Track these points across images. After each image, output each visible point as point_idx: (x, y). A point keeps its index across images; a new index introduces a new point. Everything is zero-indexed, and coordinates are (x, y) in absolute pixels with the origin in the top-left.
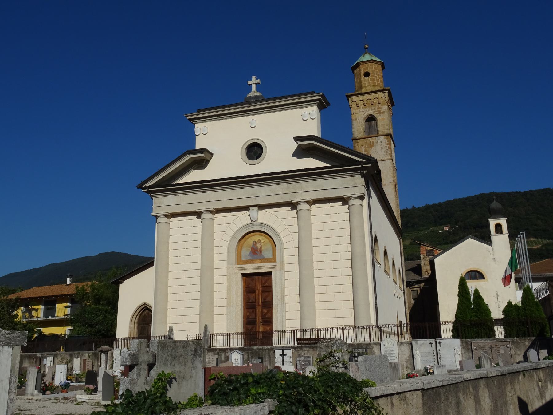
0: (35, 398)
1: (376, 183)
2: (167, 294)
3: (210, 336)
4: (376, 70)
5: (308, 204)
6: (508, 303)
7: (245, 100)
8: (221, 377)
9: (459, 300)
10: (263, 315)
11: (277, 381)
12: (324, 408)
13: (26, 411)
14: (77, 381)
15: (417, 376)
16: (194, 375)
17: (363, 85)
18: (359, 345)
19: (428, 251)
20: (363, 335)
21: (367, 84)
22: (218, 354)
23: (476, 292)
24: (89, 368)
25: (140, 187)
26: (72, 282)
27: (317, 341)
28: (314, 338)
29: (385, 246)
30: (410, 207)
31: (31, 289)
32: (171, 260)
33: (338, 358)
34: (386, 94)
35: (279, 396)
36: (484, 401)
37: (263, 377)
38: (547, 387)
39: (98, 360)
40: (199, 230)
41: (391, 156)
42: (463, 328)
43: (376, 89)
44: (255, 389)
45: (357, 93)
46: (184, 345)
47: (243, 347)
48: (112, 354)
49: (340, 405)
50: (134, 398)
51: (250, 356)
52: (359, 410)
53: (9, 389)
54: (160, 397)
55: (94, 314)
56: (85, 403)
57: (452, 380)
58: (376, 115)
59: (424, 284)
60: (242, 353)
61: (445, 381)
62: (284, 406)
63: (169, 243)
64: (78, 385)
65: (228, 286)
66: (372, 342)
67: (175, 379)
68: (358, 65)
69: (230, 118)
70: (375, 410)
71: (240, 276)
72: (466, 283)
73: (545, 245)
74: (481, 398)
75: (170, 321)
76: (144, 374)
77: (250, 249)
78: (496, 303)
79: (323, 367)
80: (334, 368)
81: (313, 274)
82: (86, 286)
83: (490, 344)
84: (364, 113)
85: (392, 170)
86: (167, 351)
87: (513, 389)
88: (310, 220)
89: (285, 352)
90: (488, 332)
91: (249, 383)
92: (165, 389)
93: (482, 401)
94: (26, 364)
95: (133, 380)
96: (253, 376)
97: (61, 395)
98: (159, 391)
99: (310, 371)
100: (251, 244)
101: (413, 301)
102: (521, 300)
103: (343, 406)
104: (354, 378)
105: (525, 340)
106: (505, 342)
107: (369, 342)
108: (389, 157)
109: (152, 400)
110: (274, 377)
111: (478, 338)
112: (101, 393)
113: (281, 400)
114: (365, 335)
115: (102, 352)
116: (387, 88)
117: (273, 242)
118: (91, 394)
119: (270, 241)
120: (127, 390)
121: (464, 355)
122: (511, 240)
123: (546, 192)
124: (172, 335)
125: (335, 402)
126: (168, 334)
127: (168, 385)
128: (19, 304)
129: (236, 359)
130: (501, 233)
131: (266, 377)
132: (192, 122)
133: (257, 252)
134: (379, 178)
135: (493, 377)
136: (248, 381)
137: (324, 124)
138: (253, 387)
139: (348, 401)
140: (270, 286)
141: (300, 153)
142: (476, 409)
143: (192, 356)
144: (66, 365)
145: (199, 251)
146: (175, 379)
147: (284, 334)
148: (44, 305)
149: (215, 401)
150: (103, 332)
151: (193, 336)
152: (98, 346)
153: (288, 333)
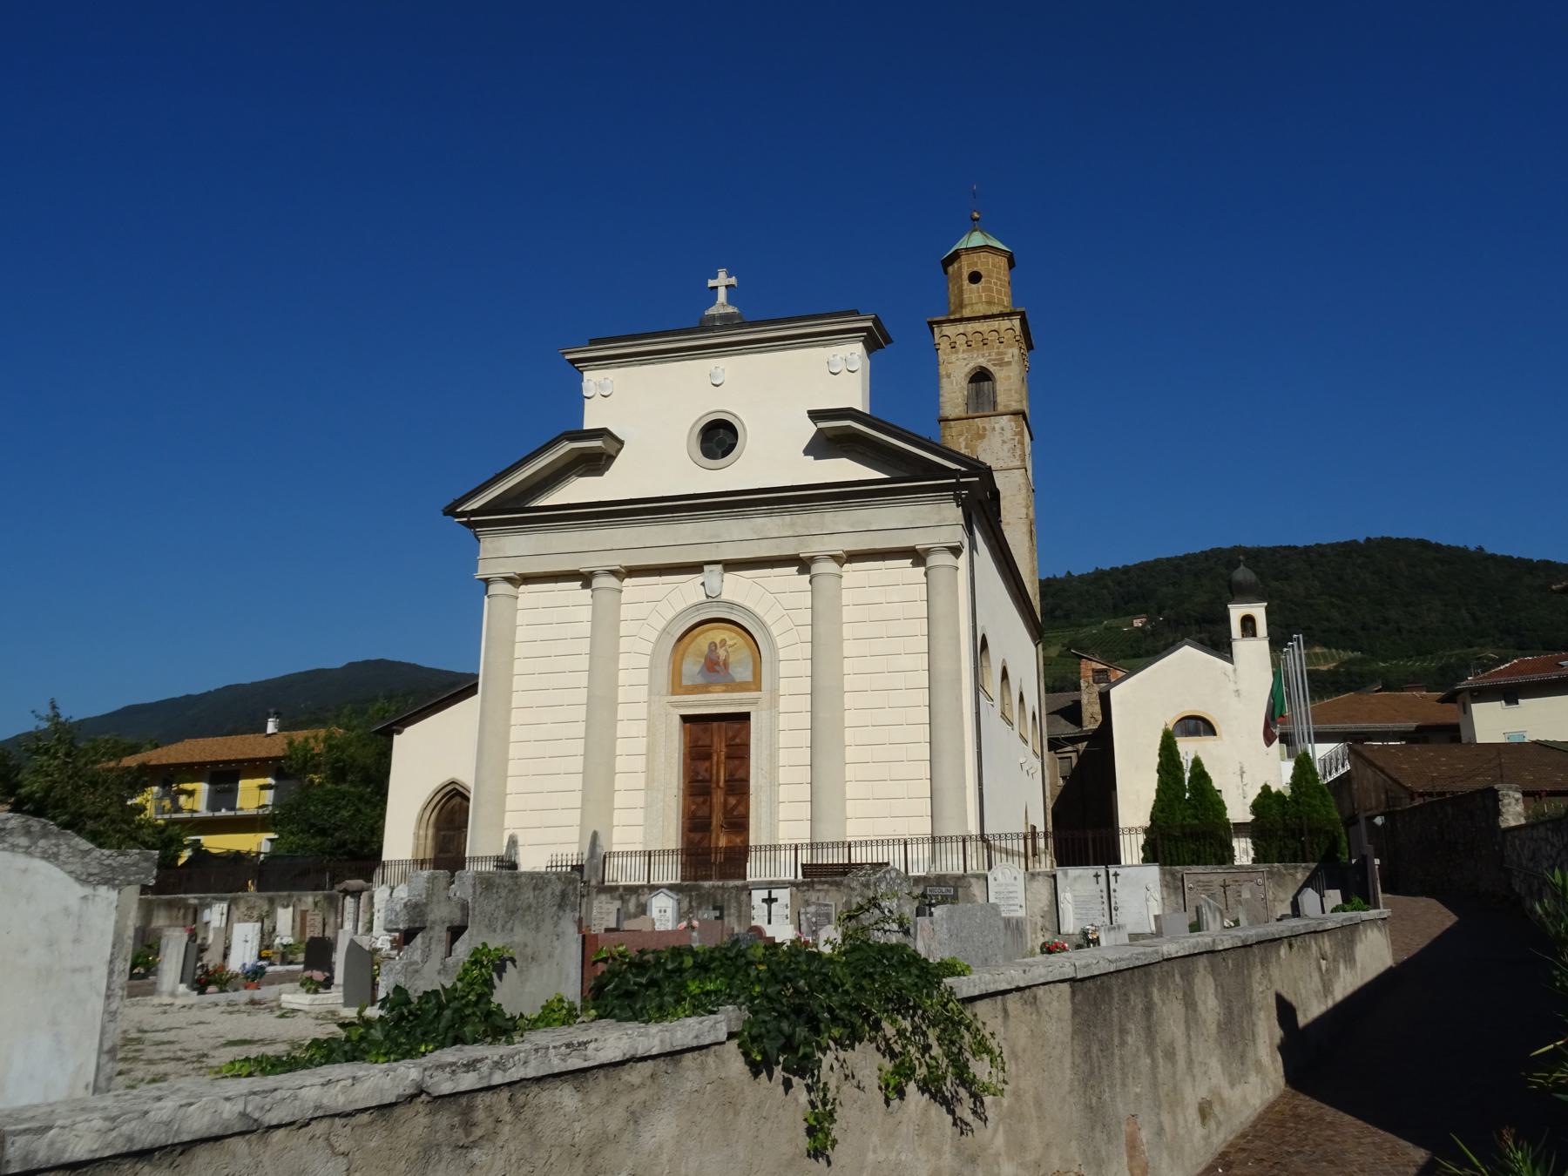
0: (179, 1002)
1: (988, 520)
2: (506, 760)
3: (605, 857)
4: (995, 269)
5: (836, 561)
6: (1262, 788)
7: (701, 322)
8: (622, 955)
9: (1159, 780)
10: (728, 812)
11: (750, 963)
12: (852, 1025)
13: (158, 1034)
14: (285, 960)
15: (1064, 949)
16: (558, 952)
17: (966, 301)
18: (941, 880)
19: (1097, 672)
20: (949, 856)
21: (974, 298)
22: (621, 897)
23: (1197, 763)
24: (314, 931)
25: (451, 511)
26: (281, 728)
27: (847, 869)
28: (841, 862)
29: (1004, 660)
30: (1061, 574)
31: (179, 744)
32: (517, 683)
33: (890, 911)
34: (1016, 322)
35: (752, 999)
36: (1205, 1003)
37: (717, 954)
38: (1337, 972)
39: (336, 913)
40: (585, 614)
41: (1024, 460)
42: (1166, 842)
43: (996, 310)
44: (697, 982)
45: (952, 317)
46: (536, 884)
47: (679, 881)
48: (371, 898)
49: (889, 1017)
50: (412, 1006)
51: (694, 904)
52: (931, 1029)
53: (108, 988)
54: (476, 1003)
55: (331, 804)
56: (300, 1014)
57: (1137, 959)
58: (992, 369)
59: (1086, 743)
60: (676, 897)
61: (1121, 960)
62: (764, 1022)
63: (513, 643)
64: (288, 971)
65: (648, 743)
66: (969, 871)
67: (513, 960)
68: (956, 256)
69: (666, 362)
70: (968, 1028)
71: (677, 721)
72: (1175, 743)
73: (1345, 663)
74: (1199, 998)
75: (512, 824)
76: (439, 950)
77: (703, 660)
78: (1238, 787)
79: (856, 931)
80: (880, 934)
81: (843, 719)
82: (313, 738)
83: (1224, 876)
84: (966, 362)
85: (1024, 491)
86: (495, 896)
87: (1267, 975)
88: (840, 597)
89: (775, 893)
90: (1220, 853)
91: (686, 970)
92: (489, 984)
93: (1200, 1003)
94: (160, 920)
95: (412, 964)
96: (693, 953)
97: (243, 995)
98: (473, 989)
99: (828, 939)
100: (705, 649)
101: (1061, 782)
102: (1289, 781)
103: (896, 1020)
104: (923, 956)
105: (1296, 868)
106: (1254, 874)
107: (961, 871)
108: (1018, 463)
109: (456, 1011)
110: (744, 956)
111: (1198, 864)
112: (341, 989)
113: (756, 1008)
114: (955, 856)
115: (346, 892)
116: (1018, 310)
117: (754, 646)
118: (316, 992)
119: (746, 641)
120: (398, 989)
121: (1166, 901)
122: (1275, 651)
123: (1548, 568)
124: (516, 854)
125: (879, 1011)
126: (506, 853)
127: (495, 975)
128: (146, 779)
129: (663, 913)
130: (1254, 635)
131: (725, 955)
132: (577, 368)
133: (717, 668)
134: (995, 509)
135: (1225, 950)
136: (684, 966)
137: (878, 383)
138: (694, 979)
139: (910, 1007)
140: (746, 746)
141: (823, 446)
142: (1187, 1021)
143: (555, 908)
144: (258, 925)
145: (584, 663)
146: (513, 960)
147: (773, 853)
148: (211, 782)
149: (605, 1011)
150: (351, 847)
151: (564, 857)
152: (337, 880)
153: (783, 852)
